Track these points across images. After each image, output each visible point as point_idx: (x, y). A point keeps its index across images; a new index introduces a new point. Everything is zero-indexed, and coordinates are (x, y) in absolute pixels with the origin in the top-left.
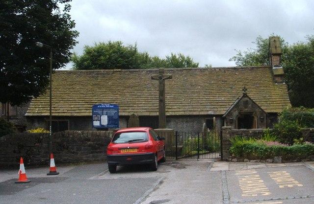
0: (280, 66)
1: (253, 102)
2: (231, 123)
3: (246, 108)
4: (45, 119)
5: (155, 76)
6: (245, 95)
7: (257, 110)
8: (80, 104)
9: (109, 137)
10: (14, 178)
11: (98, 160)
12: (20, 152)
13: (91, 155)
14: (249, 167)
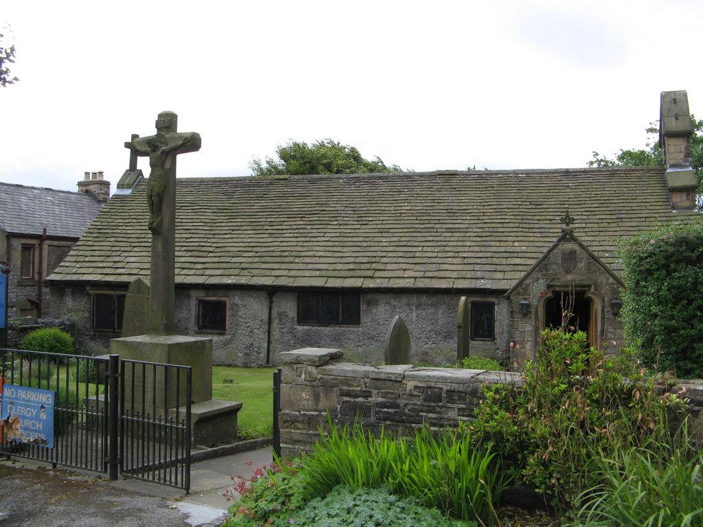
0: (686, 166)
1: (592, 256)
2: (525, 315)
3: (568, 272)
6: (567, 236)
7: (603, 279)
10: (452, 388)
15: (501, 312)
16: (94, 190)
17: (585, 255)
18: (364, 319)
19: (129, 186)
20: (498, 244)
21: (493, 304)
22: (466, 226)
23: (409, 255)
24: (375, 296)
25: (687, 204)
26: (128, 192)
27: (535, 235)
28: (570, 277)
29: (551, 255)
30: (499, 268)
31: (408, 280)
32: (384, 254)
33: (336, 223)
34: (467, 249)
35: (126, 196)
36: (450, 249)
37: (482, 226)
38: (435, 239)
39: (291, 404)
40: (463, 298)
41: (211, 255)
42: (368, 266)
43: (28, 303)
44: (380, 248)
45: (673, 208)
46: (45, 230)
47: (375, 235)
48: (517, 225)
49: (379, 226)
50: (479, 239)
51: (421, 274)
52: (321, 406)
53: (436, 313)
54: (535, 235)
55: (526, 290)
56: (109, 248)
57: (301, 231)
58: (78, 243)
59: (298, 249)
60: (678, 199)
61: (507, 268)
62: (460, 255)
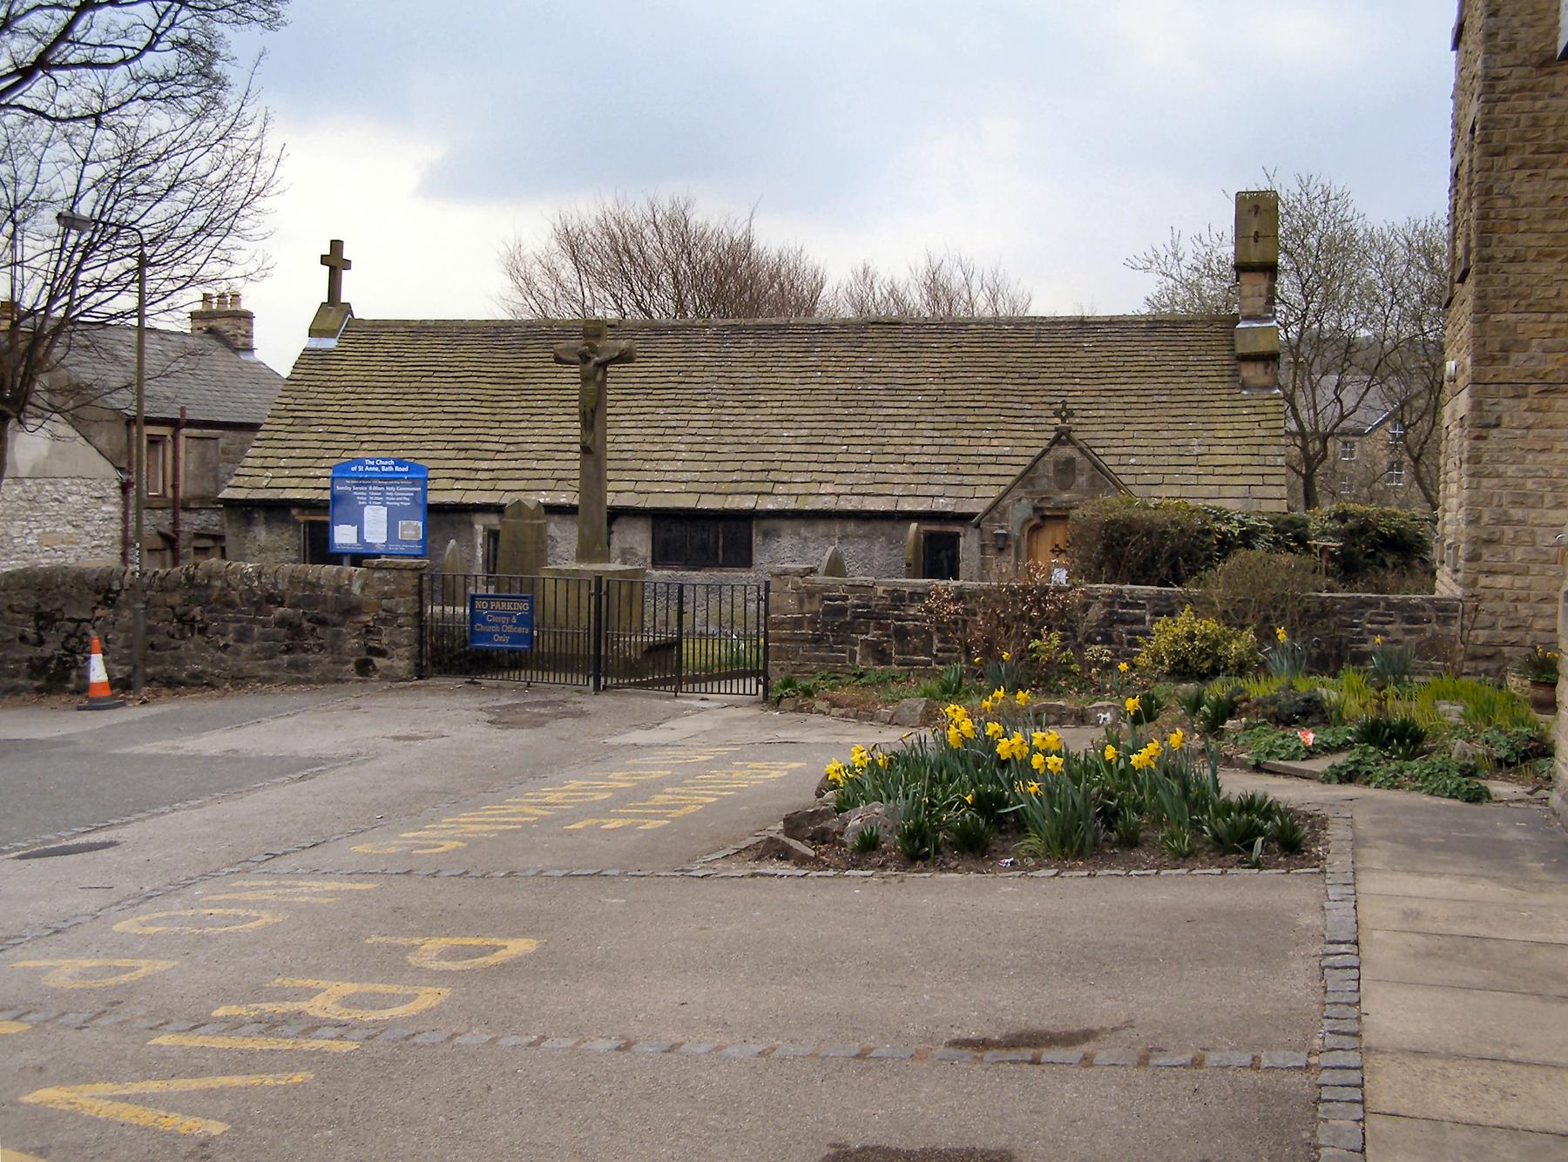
1: (1098, 467)
2: (1001, 550)
4: (294, 512)
5: (567, 350)
6: (1062, 437)
8: (983, 470)
9: (348, 592)
11: (308, 681)
12: (41, 642)
13: (286, 657)
14: (423, 702)
15: (969, 545)
16: (226, 328)
17: (1087, 465)
18: (757, 558)
19: (331, 334)
20: (966, 442)
21: (957, 535)
22: (916, 412)
23: (828, 458)
24: (776, 523)
25: (1265, 380)
26: (331, 343)
27: (1026, 427)
28: (1066, 496)
29: (1040, 464)
30: (967, 480)
31: (827, 498)
32: (787, 457)
33: (704, 404)
34: (917, 449)
35: (329, 351)
36: (891, 449)
37: (943, 412)
38: (868, 432)
39: (778, 609)
40: (914, 526)
41: (499, 456)
42: (762, 476)
43: (159, 539)
44: (780, 448)
45: (1244, 387)
46: (183, 410)
47: (771, 425)
48: (997, 411)
49: (775, 411)
50: (937, 434)
51: (847, 489)
52: (806, 609)
53: (870, 549)
54: (1026, 427)
55: (1002, 514)
56: (318, 444)
57: (647, 417)
58: (259, 435)
59: (647, 447)
60: (1250, 372)
61: (977, 480)
62: (908, 458)
